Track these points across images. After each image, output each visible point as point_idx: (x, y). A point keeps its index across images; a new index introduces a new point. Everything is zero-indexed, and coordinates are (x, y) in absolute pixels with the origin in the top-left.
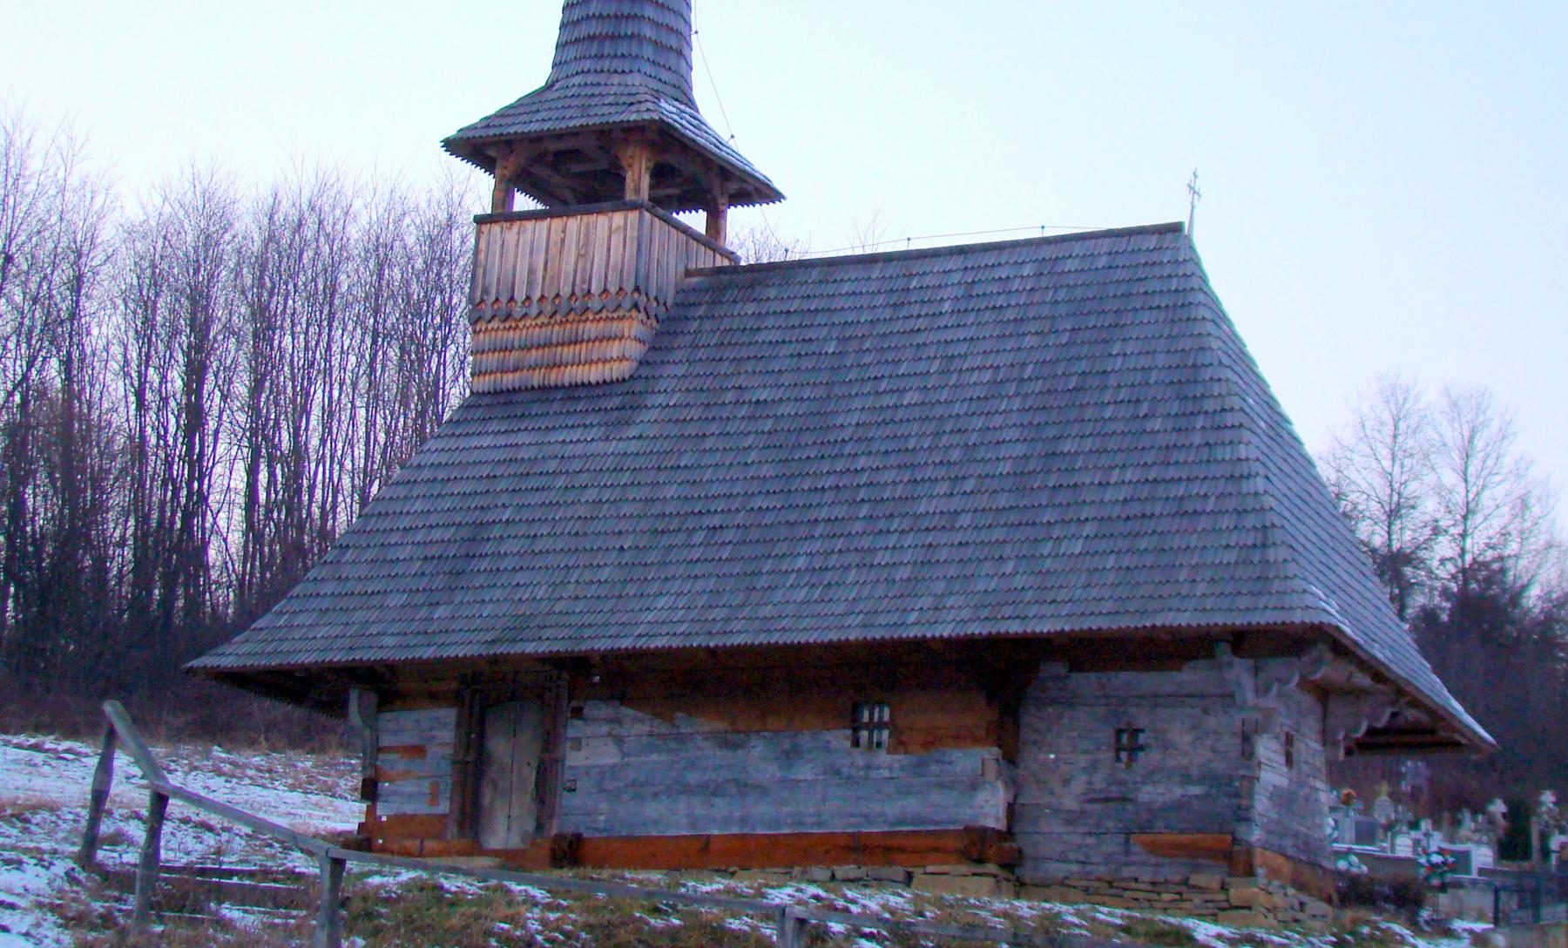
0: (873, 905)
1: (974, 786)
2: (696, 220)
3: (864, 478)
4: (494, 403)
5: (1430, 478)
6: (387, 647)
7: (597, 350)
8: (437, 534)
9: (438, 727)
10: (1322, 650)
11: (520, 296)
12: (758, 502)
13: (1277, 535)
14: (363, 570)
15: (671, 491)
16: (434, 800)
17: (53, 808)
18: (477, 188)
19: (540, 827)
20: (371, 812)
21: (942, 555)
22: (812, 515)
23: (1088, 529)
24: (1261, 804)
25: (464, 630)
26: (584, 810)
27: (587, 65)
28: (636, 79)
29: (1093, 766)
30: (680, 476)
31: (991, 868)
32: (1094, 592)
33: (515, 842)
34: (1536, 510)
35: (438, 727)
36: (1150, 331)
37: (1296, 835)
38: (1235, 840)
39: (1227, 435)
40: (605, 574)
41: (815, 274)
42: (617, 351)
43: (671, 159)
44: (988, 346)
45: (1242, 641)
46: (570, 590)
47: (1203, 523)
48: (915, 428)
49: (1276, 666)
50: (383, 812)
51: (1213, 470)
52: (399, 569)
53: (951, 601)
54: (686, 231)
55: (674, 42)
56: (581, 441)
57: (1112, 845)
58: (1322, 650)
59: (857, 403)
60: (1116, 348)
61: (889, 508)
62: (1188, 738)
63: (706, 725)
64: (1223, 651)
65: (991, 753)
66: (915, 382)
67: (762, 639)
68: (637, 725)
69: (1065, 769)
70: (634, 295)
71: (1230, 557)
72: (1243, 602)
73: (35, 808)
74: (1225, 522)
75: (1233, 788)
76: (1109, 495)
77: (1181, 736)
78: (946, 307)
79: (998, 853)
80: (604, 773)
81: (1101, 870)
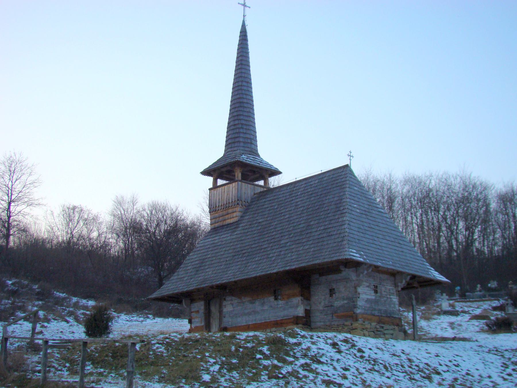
1: (297, 307)
2: (261, 183)
7: (231, 216)
12: (253, 246)
16: (201, 323)
18: (209, 181)
19: (220, 326)
20: (191, 326)
26: (228, 321)
29: (325, 299)
35: (199, 306)
38: (354, 313)
41: (277, 190)
42: (235, 215)
50: (193, 326)
57: (330, 317)
64: (342, 268)
65: (299, 298)
68: (236, 301)
75: (353, 300)
81: (328, 323)
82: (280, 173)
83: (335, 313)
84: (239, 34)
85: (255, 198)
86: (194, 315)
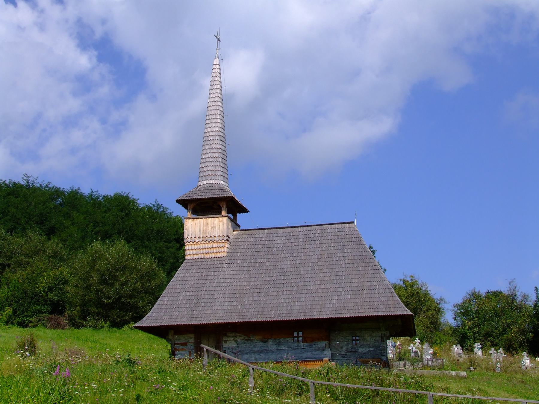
1: (323, 350)
35: (191, 339)
68: (240, 339)
82: (178, 201)
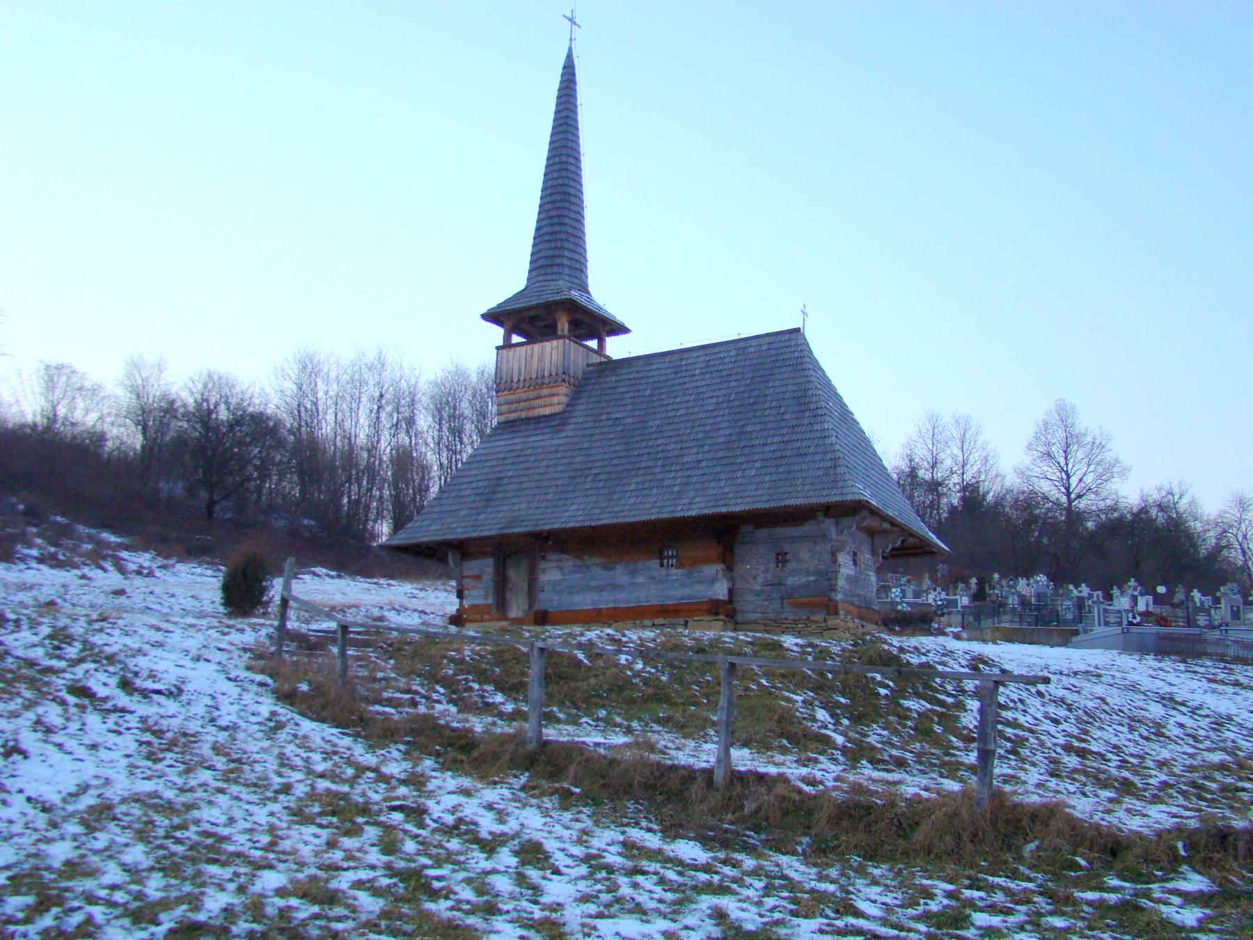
0: (635, 637)
1: (713, 581)
2: (593, 344)
3: (661, 448)
4: (508, 427)
5: (948, 451)
6: (459, 532)
7: (548, 401)
8: (481, 484)
9: (486, 567)
10: (865, 513)
11: (515, 380)
12: (615, 462)
13: (841, 462)
14: (451, 501)
15: (578, 459)
17: (357, 607)
18: (496, 334)
19: (530, 607)
20: (461, 604)
21: (694, 479)
22: (637, 466)
23: (758, 465)
24: (841, 582)
25: (490, 525)
26: (549, 600)
27: (540, 278)
28: (561, 282)
29: (766, 571)
30: (582, 453)
31: (722, 617)
32: (760, 492)
33: (520, 614)
34: (991, 462)
35: (486, 567)
36: (785, 376)
37: (859, 596)
38: (830, 600)
39: (819, 419)
40: (549, 497)
41: (641, 362)
42: (557, 401)
43: (578, 316)
44: (715, 387)
45: (829, 510)
46: (535, 505)
47: (808, 459)
48: (682, 425)
49: (846, 521)
50: (466, 604)
51: (813, 435)
52: (465, 499)
53: (697, 500)
54: (587, 347)
55: (578, 266)
56: (542, 440)
57: (776, 605)
58: (865, 513)
59: (658, 416)
60: (771, 384)
61: (670, 461)
62: (808, 555)
63: (596, 560)
65: (720, 567)
66: (684, 405)
67: (615, 521)
68: (569, 562)
69: (753, 572)
70: (563, 376)
71: (820, 473)
72: (825, 493)
73: (350, 607)
74: (818, 458)
75: (828, 575)
76: (767, 449)
77: (804, 555)
78: (697, 372)
79: (726, 611)
80: (555, 583)
81: (771, 616)
83: (789, 597)
84: (560, 71)
85: (591, 372)
86: (468, 582)
